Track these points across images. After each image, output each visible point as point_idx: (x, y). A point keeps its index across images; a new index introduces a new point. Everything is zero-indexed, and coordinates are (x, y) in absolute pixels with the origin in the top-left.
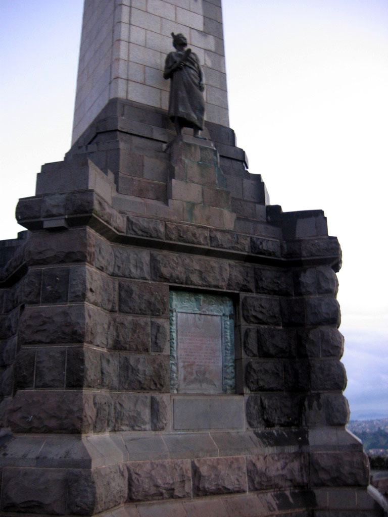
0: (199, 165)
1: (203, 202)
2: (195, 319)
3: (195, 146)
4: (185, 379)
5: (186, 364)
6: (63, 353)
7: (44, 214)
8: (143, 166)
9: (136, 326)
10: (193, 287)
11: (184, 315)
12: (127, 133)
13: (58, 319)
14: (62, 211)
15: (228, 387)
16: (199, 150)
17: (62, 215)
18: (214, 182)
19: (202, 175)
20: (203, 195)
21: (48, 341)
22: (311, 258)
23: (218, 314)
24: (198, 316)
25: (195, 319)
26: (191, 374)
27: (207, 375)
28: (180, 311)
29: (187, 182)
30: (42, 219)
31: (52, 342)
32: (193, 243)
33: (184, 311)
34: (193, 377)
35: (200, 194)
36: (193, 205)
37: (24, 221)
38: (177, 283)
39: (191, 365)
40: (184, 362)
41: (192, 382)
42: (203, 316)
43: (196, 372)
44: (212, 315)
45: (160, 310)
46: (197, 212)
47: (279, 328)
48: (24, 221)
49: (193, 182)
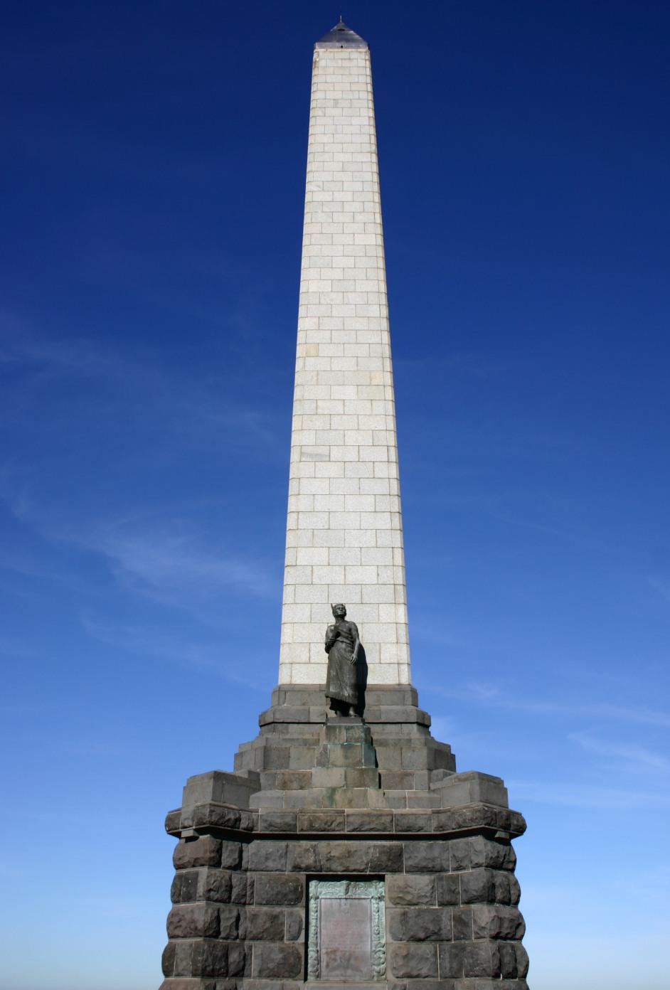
0: (342, 746)
1: (346, 784)
2: (340, 905)
3: (340, 727)
4: (327, 966)
5: (330, 950)
6: (191, 945)
7: (180, 826)
8: (289, 757)
9: (375, 919)
10: (331, 873)
11: (329, 901)
12: (283, 723)
13: (188, 917)
14: (190, 823)
15: (375, 973)
16: (344, 732)
17: (191, 826)
18: (360, 761)
19: (346, 757)
20: (345, 777)
21: (182, 935)
22: (460, 830)
23: (366, 897)
24: (343, 901)
25: (340, 905)
26: (335, 960)
27: (352, 962)
28: (323, 897)
29: (328, 768)
30: (180, 830)
31: (184, 937)
32: (328, 831)
33: (328, 897)
34: (336, 964)
35: (343, 777)
36: (334, 790)
37: (170, 832)
38: (313, 871)
39: (334, 951)
40: (327, 948)
41: (335, 968)
42: (349, 901)
43: (340, 958)
44: (359, 899)
45: (302, 897)
46: (338, 797)
47: (434, 908)
48: (170, 832)
49: (336, 766)
